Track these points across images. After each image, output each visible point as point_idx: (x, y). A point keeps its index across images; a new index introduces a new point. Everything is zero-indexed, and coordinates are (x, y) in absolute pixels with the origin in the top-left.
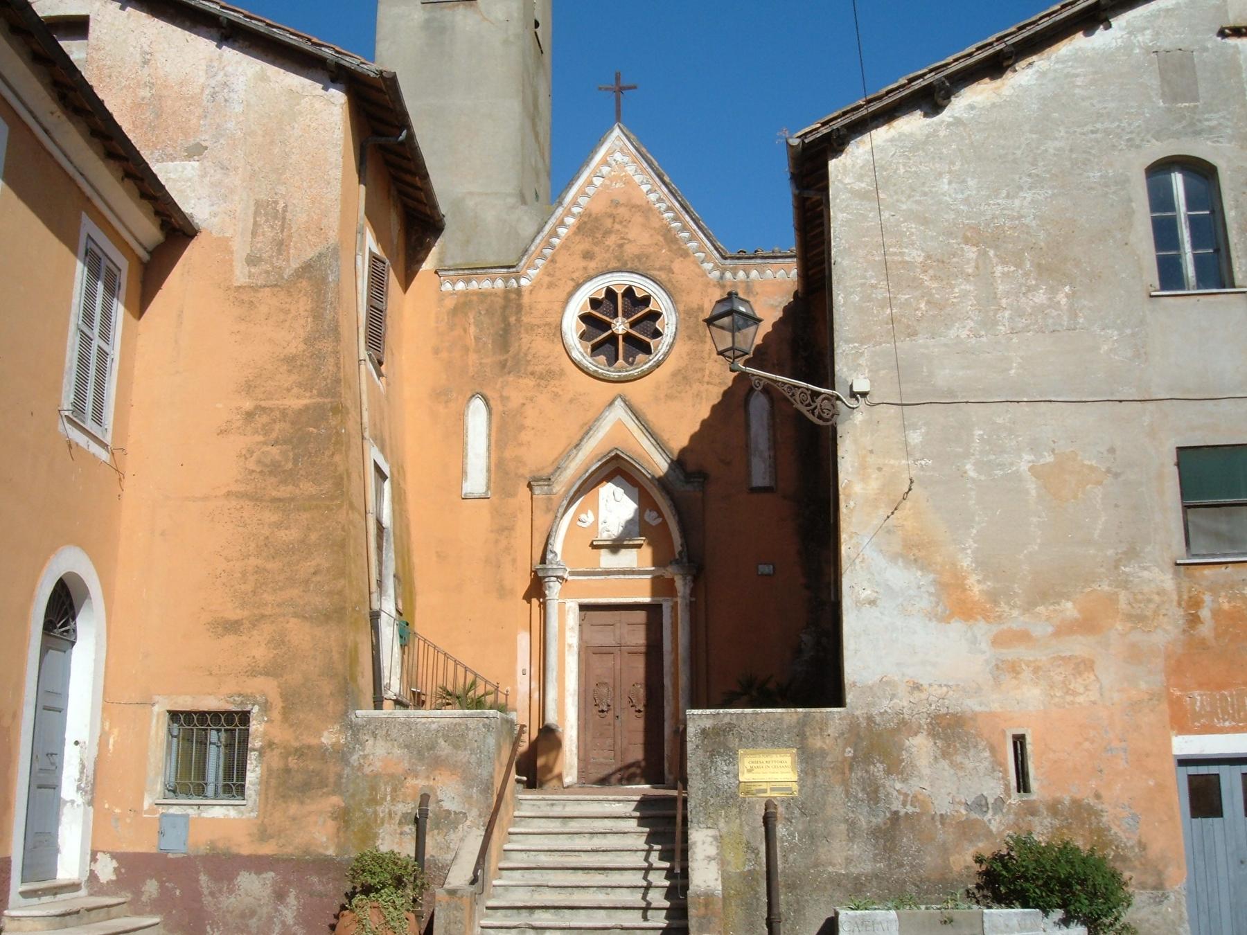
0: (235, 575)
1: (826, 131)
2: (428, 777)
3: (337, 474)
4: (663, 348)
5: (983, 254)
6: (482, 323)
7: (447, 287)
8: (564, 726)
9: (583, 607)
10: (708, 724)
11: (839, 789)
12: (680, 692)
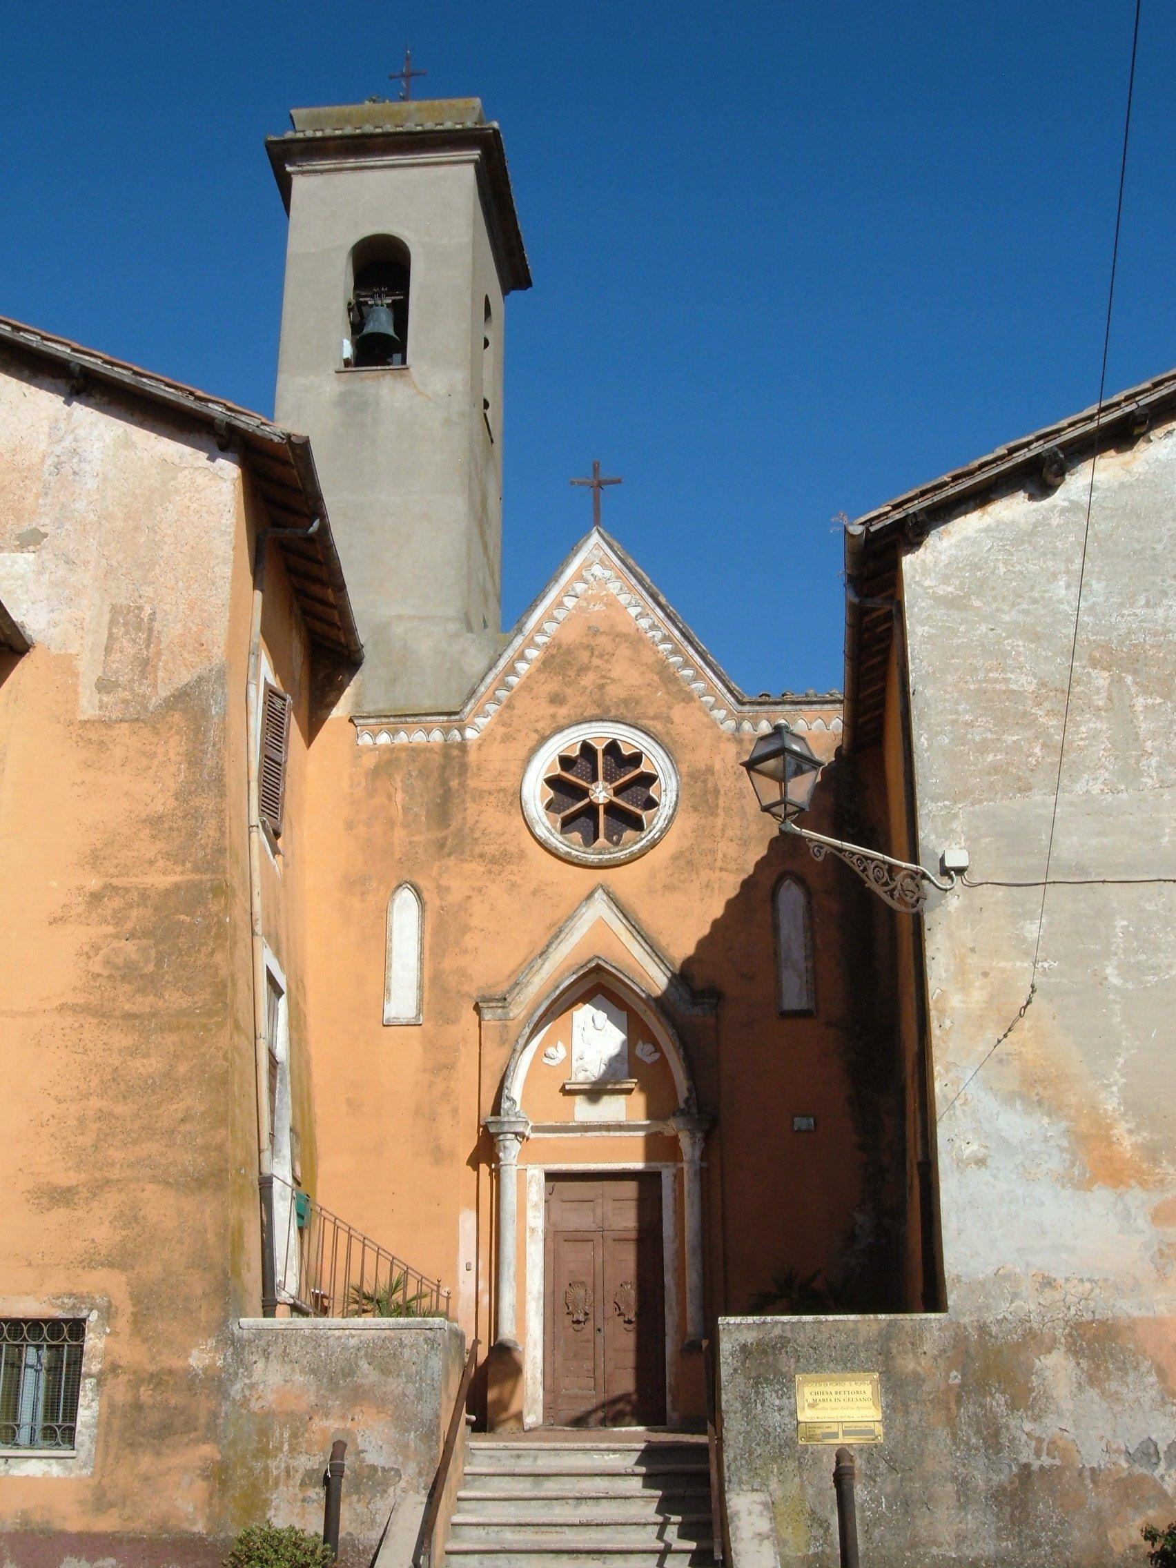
0: (69, 1122)
1: (898, 517)
2: (343, 1417)
3: (219, 979)
4: (660, 823)
5: (1117, 681)
7: (366, 740)
8: (524, 1343)
9: (551, 1177)
10: (750, 1337)
11: (943, 1432)
12: (688, 1295)
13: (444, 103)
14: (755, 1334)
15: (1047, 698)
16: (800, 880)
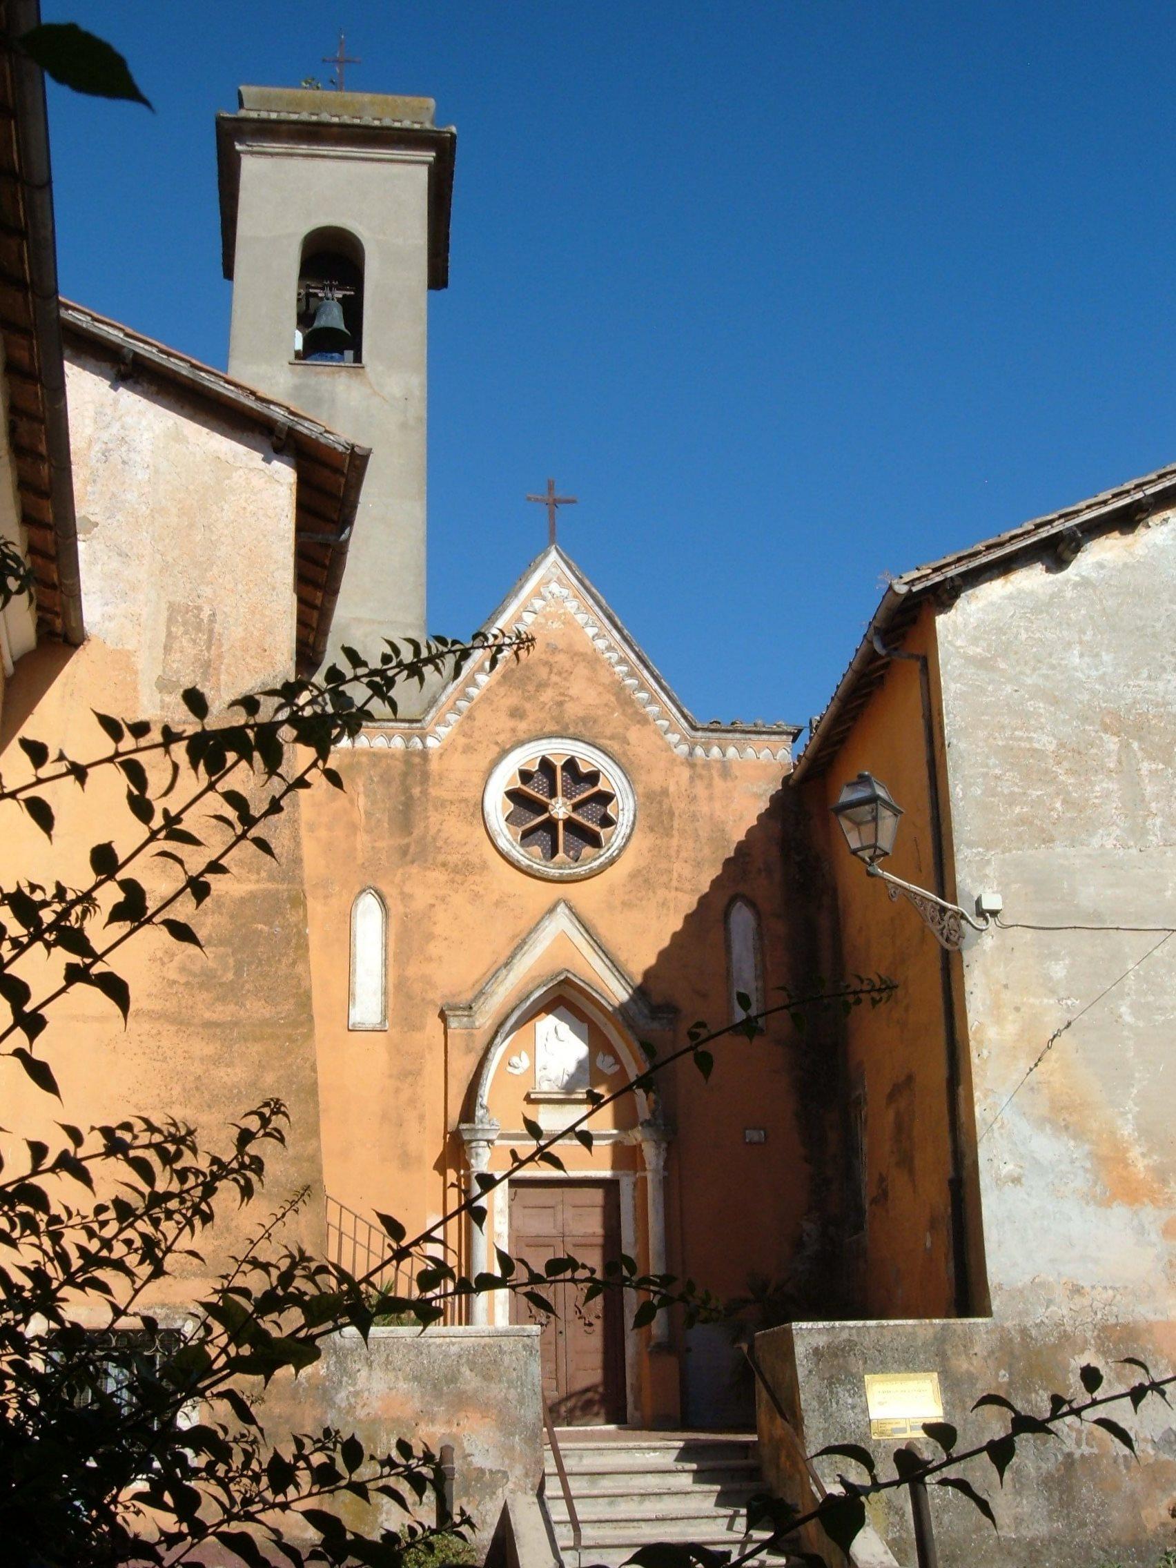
1: (938, 579)
2: (449, 1422)
3: (302, 990)
4: (618, 842)
5: (1126, 746)
6: (375, 793)
10: (821, 1341)
13: (400, 100)
14: (825, 1338)
15: (1066, 758)
16: (751, 903)
